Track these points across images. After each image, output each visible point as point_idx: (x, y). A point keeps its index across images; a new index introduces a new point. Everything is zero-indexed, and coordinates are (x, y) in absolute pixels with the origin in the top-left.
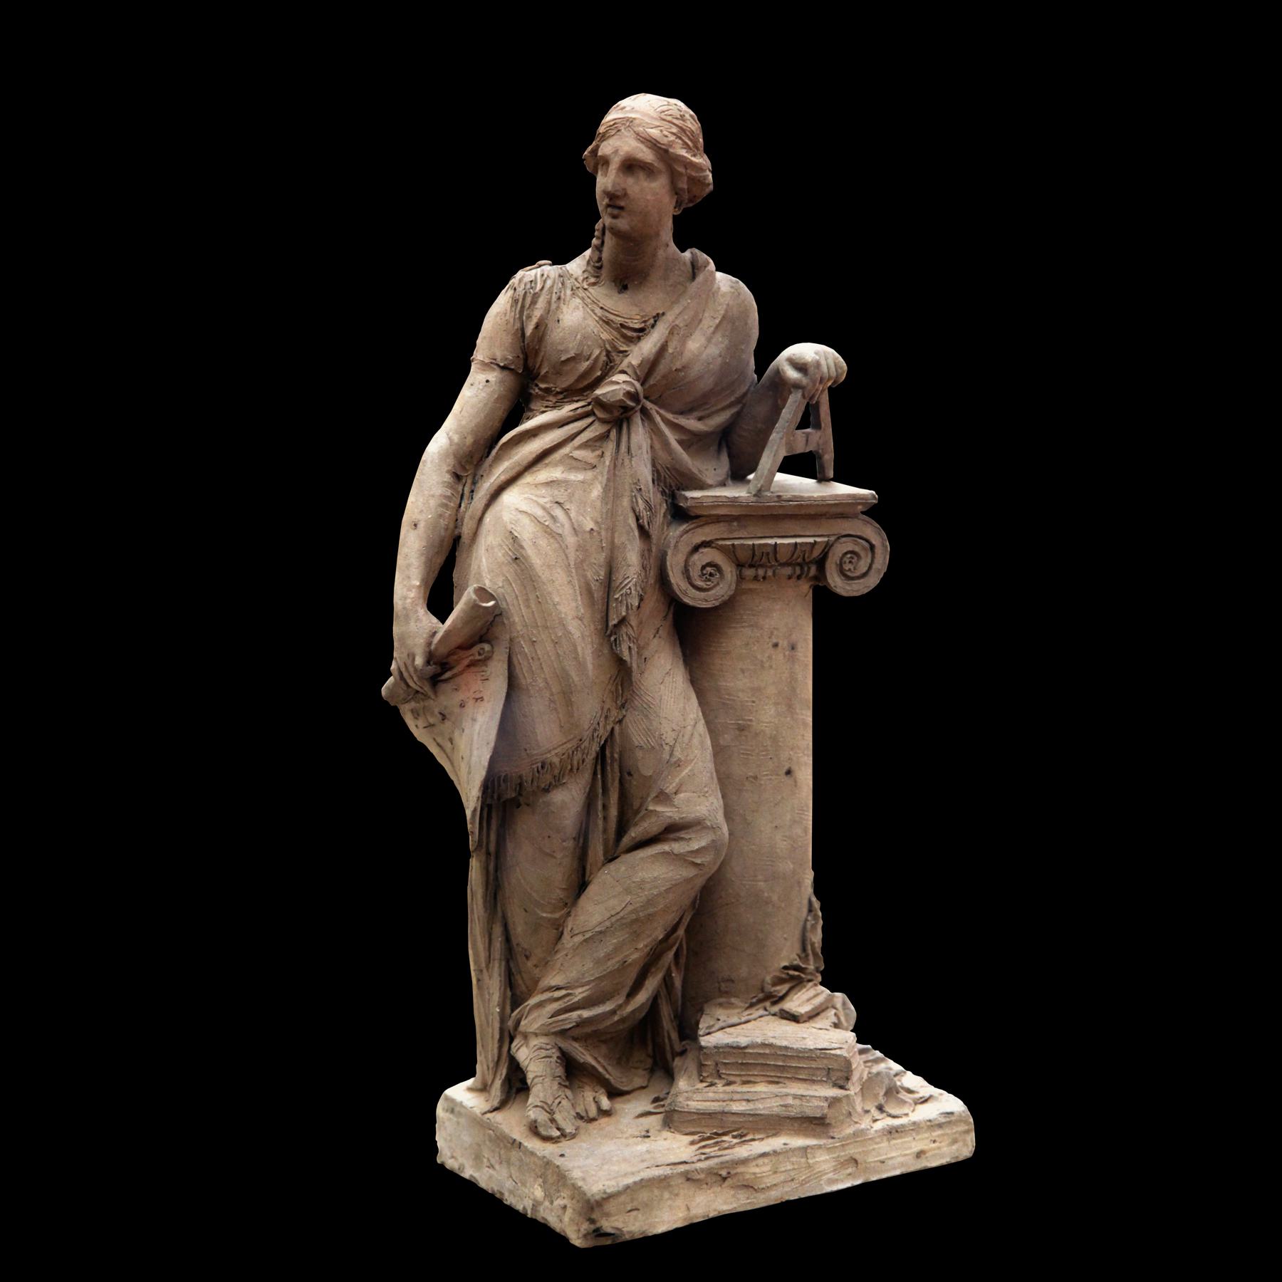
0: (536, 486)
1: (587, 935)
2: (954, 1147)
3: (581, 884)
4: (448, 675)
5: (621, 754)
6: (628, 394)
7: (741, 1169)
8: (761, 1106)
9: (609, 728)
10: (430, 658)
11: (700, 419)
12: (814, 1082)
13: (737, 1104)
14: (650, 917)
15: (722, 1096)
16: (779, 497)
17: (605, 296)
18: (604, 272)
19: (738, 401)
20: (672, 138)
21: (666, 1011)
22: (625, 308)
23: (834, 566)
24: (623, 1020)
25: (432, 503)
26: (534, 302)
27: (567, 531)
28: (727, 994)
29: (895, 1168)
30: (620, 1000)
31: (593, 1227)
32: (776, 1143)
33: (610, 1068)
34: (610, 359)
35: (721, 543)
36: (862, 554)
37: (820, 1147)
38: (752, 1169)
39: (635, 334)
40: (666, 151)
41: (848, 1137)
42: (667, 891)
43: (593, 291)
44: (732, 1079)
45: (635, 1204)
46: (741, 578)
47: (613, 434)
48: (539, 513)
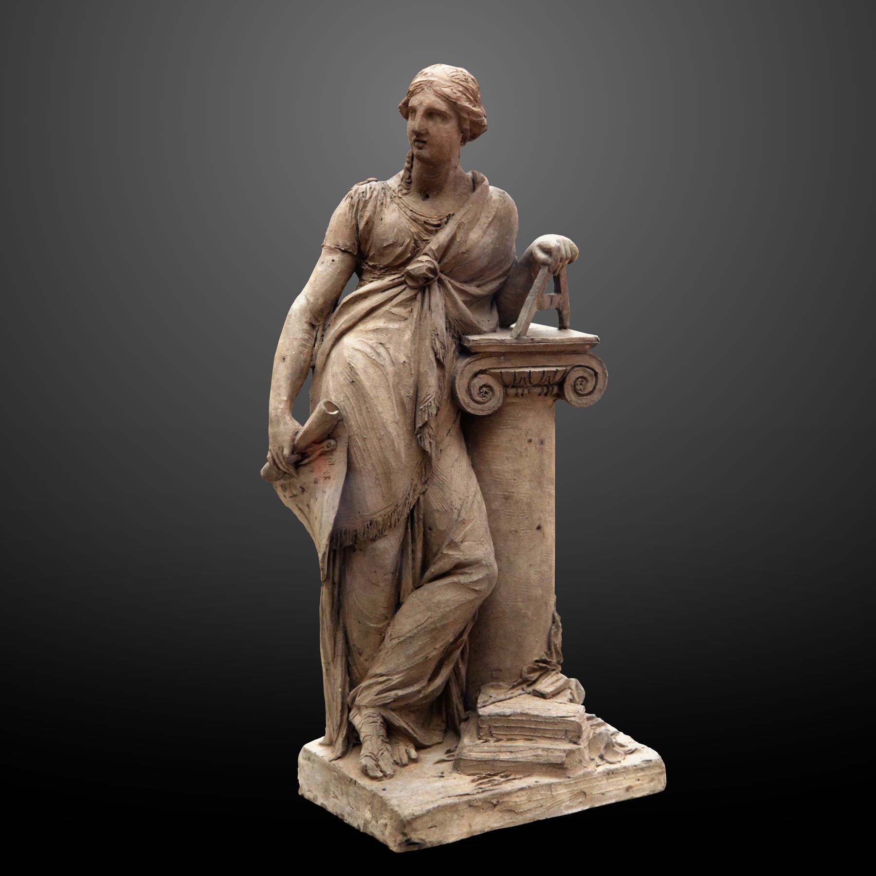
0: (366, 332)
1: (401, 639)
2: (652, 784)
3: (397, 604)
4: (306, 461)
5: (424, 515)
6: (429, 269)
7: (506, 799)
8: (520, 756)
9: (416, 497)
10: (294, 449)
11: (478, 286)
12: (556, 739)
13: (504, 754)
14: (444, 627)
15: (493, 749)
16: (532, 339)
17: (414, 203)
18: (413, 186)
19: (505, 274)
20: (459, 94)
21: (455, 691)
22: (427, 210)
23: (570, 387)
24: (425, 697)
25: (296, 343)
26: (365, 207)
27: (387, 363)
28: (497, 679)
29: (611, 798)
30: (424, 683)
31: (405, 838)
32: (530, 781)
33: (416, 730)
34: (417, 245)
35: (492, 371)
36: (589, 378)
37: (560, 784)
38: (514, 799)
39: (434, 228)
40: (455, 103)
41: (579, 777)
42: (456, 609)
43: (405, 199)
44: (500, 737)
45: (434, 823)
46: (506, 395)
47: (419, 296)
48: (368, 350)
